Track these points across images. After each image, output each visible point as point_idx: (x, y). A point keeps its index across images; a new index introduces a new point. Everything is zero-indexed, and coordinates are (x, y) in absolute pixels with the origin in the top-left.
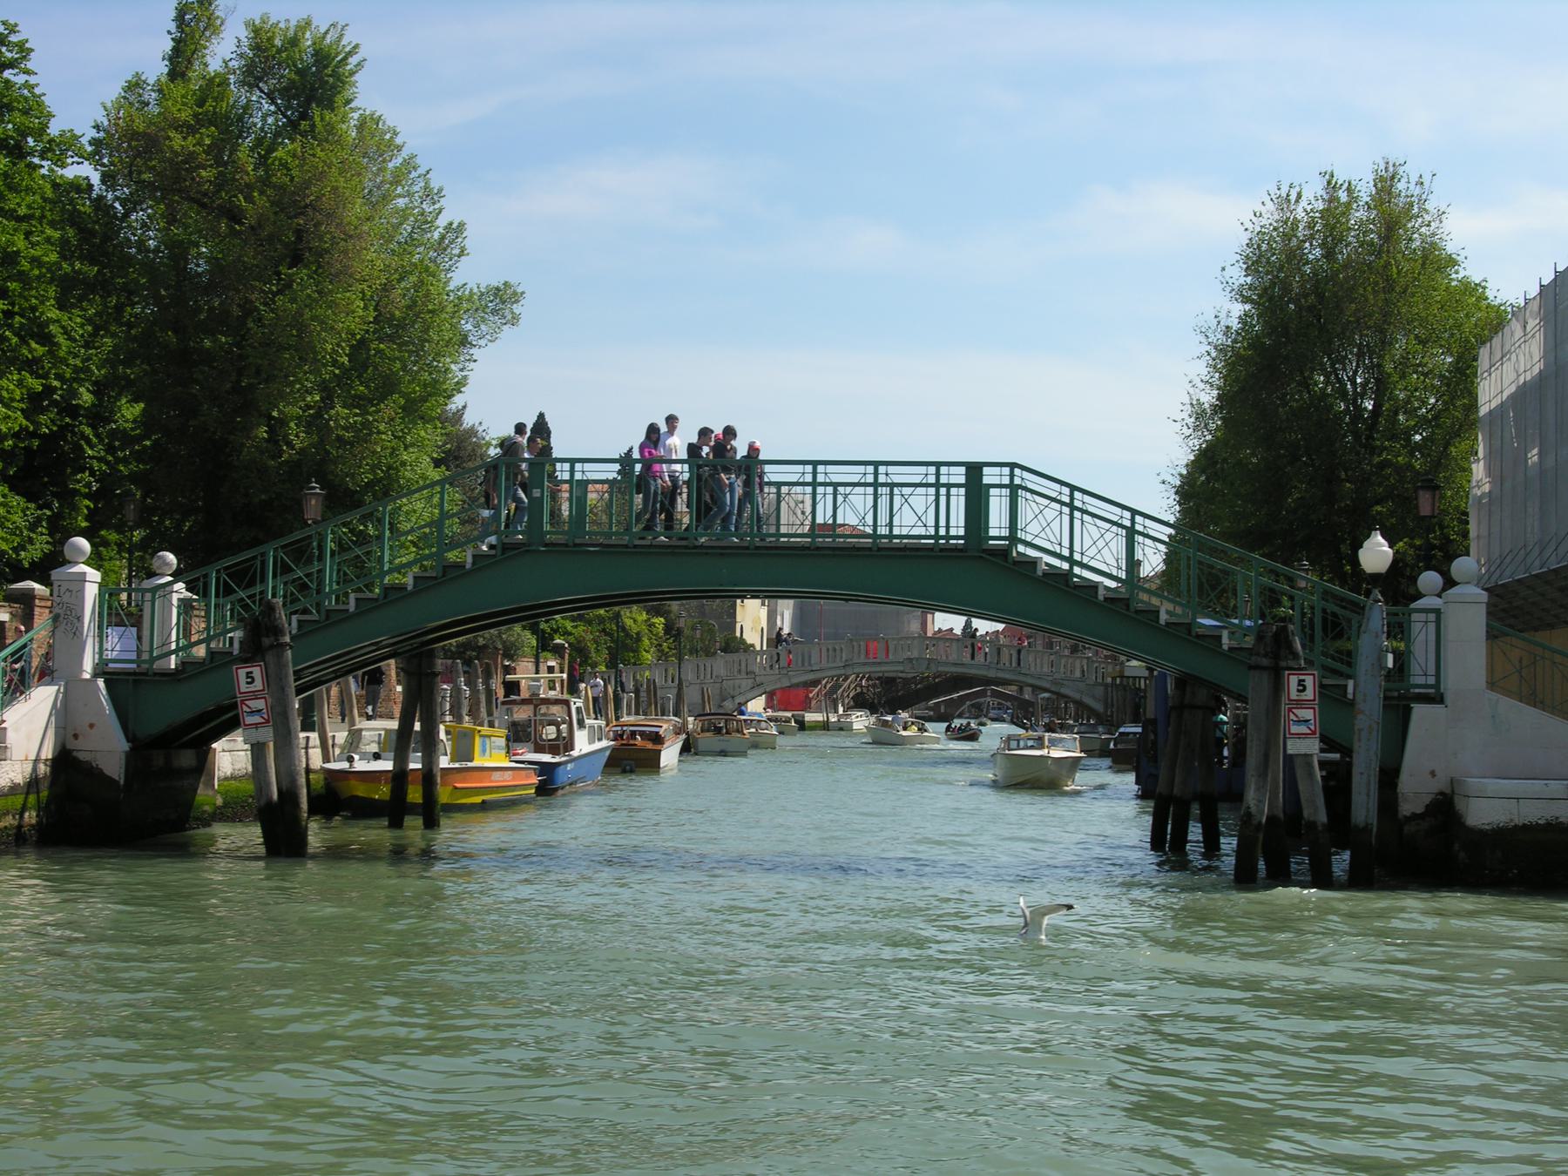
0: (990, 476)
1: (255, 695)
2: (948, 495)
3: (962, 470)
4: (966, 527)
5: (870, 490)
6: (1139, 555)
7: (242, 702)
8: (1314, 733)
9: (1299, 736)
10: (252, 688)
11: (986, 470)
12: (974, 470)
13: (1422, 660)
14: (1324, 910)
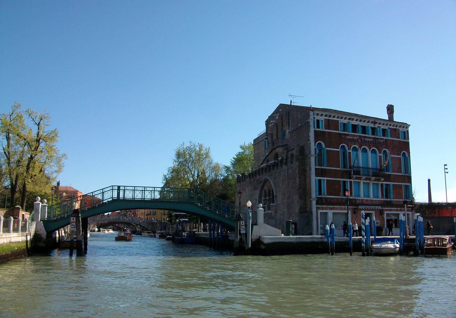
0: (121, 188)
12: (119, 187)
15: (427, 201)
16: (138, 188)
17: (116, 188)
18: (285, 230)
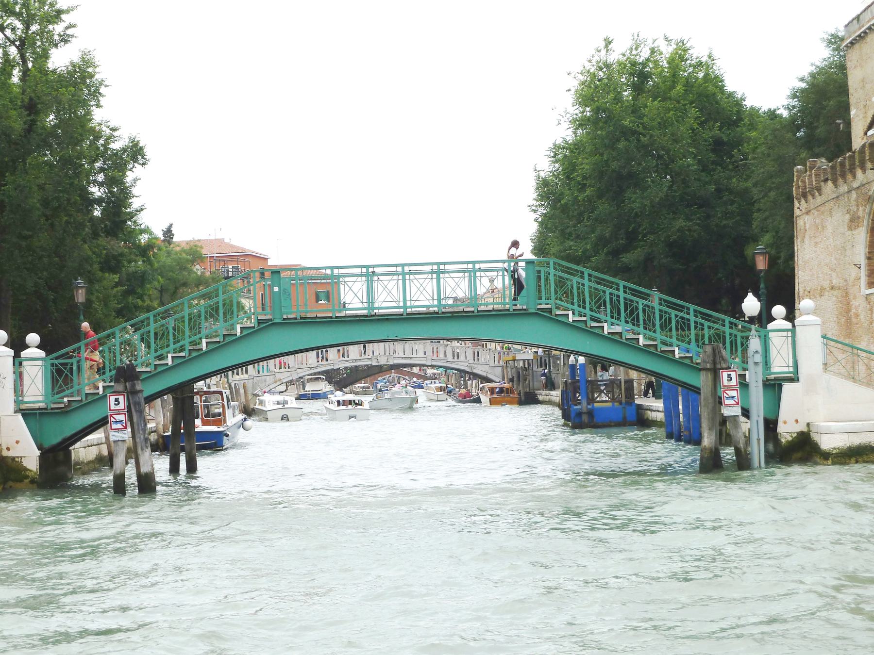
1: (730, 388)
7: (111, 415)
8: (738, 403)
9: (730, 405)
10: (118, 407)
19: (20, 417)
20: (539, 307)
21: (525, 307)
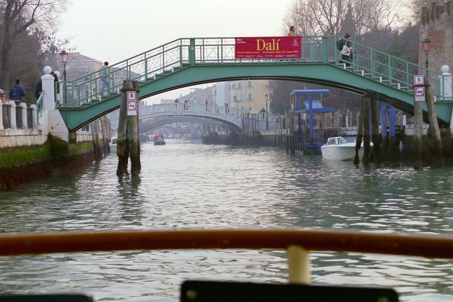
0: (197, 42)
2: (222, 48)
3: (189, 40)
4: (189, 58)
5: (224, 47)
6: (98, 70)
10: (132, 98)
11: (196, 40)
12: (193, 40)
13: (448, 84)
14: (245, 157)
15: (196, 44)
16: (210, 42)
17: (188, 42)
18: (301, 121)
19: (58, 111)
20: (329, 61)
21: (321, 61)
